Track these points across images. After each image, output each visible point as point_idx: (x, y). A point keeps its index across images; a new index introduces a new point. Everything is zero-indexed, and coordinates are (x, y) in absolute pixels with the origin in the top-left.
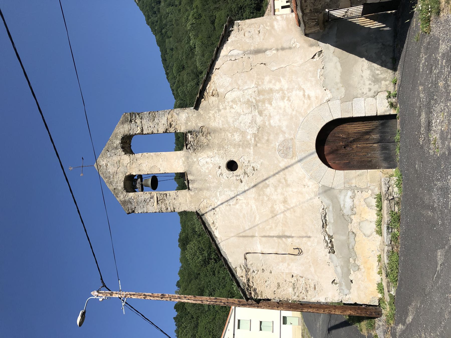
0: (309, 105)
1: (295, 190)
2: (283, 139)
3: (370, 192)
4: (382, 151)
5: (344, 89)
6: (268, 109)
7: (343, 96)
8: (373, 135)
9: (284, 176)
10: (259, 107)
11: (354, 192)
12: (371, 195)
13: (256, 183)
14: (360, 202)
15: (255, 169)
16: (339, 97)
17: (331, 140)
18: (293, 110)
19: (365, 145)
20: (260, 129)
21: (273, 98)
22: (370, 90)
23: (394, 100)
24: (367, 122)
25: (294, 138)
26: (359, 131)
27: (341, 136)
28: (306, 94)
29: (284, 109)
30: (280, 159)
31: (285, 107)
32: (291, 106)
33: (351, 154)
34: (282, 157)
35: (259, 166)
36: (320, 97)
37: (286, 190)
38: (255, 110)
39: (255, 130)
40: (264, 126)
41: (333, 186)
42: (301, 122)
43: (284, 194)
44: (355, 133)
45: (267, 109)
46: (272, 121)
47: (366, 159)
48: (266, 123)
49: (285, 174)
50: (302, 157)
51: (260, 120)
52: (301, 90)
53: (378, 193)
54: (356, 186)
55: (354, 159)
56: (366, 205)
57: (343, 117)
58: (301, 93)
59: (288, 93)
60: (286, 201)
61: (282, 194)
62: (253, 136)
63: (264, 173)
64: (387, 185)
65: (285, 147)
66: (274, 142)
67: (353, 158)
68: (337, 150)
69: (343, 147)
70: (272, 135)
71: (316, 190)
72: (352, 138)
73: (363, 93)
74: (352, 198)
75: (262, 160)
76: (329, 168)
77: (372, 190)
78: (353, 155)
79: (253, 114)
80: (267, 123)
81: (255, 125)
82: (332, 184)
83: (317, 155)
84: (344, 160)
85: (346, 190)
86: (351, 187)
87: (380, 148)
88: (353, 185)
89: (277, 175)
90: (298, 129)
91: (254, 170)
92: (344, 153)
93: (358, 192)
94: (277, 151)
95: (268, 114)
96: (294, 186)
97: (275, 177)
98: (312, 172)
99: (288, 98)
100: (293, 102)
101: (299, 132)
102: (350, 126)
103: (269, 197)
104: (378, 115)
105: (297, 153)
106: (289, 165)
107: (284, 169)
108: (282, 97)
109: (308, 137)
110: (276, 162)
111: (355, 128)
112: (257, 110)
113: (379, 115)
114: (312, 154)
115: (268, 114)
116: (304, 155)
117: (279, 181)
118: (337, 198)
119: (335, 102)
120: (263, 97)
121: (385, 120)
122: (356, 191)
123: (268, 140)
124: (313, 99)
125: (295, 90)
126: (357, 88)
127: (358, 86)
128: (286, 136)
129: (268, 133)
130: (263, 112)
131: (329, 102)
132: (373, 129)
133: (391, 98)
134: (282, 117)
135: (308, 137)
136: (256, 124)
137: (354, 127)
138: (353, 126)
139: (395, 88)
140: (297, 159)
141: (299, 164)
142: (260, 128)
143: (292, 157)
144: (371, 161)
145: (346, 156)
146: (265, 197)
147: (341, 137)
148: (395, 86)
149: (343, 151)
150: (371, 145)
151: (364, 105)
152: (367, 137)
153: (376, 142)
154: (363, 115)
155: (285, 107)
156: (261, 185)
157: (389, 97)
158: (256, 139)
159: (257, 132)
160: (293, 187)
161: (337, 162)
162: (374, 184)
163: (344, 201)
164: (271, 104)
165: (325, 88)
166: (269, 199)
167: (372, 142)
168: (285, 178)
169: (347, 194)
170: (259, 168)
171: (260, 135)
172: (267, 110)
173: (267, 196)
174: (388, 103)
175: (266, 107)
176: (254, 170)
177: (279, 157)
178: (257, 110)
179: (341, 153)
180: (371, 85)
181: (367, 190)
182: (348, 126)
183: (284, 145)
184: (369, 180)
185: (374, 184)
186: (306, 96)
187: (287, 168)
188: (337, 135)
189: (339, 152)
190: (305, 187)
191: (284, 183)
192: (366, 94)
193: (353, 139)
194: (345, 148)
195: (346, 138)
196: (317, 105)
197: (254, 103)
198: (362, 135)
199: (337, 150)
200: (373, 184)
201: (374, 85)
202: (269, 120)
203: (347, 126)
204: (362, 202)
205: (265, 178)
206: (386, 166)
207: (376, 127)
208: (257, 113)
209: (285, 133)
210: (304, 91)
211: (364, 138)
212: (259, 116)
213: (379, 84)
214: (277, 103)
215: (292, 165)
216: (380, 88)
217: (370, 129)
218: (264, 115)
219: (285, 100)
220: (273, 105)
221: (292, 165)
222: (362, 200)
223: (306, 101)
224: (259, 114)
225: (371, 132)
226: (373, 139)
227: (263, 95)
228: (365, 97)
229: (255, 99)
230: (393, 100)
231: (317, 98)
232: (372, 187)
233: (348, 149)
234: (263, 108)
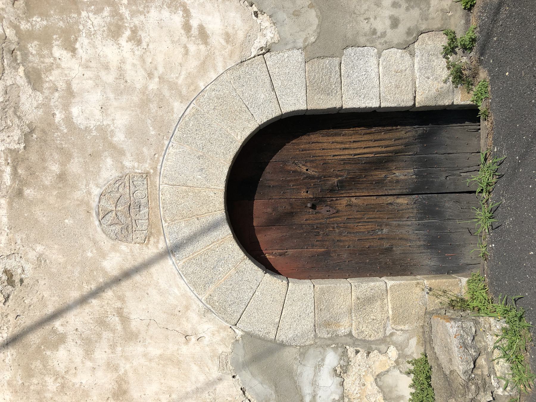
0: (204, 61)
1: (154, 351)
2: (115, 174)
3: (393, 352)
4: (421, 219)
5: (317, 16)
6: (63, 65)
7: (312, 39)
8: (397, 168)
9: (119, 304)
10: (31, 58)
11: (345, 353)
12: (397, 362)
13: (17, 330)
14: (364, 385)
15: (16, 279)
16: (301, 40)
17: (272, 183)
18: (150, 75)
19: (373, 200)
20: (35, 136)
21: (81, 27)
22: (395, 23)
23: (464, 59)
24: (380, 128)
25: (152, 171)
26: (355, 155)
27: (304, 169)
28: (194, 23)
29: (120, 69)
30: (106, 243)
31: (123, 61)
32: (142, 59)
33: (334, 228)
34: (114, 237)
35: (28, 267)
36: (241, 35)
37: (123, 351)
38: (14, 68)
39: (16, 138)
40: (50, 125)
41: (282, 337)
42: (176, 116)
43: (116, 368)
44: (346, 162)
45: (58, 66)
46: (75, 111)
47: (375, 244)
48: (54, 115)
49: (121, 299)
50: (180, 236)
51: (35, 104)
52: (176, 9)
53: (417, 356)
54: (350, 334)
55: (342, 244)
56: (381, 395)
57: (313, 106)
58: (178, 19)
59: (133, 14)
60: (125, 392)
61: (111, 366)
62: (6, 160)
63: (46, 294)
64: (472, 352)
65: (122, 200)
66: (84, 183)
67: (338, 238)
68: (291, 214)
69: (309, 205)
70: (76, 160)
71: (224, 349)
72: (337, 176)
73: (374, 32)
74: (338, 372)
75: (39, 248)
76: (268, 275)
77: (400, 347)
78: (337, 231)
79: (9, 83)
80: (59, 117)
81: (16, 121)
82: (275, 329)
83: (230, 232)
84: (313, 246)
85: (321, 349)
86: (337, 336)
87: (415, 211)
88: (343, 331)
89: (94, 302)
90: (166, 143)
91: (11, 282)
92: (312, 225)
93: (357, 352)
94: (94, 214)
95: (62, 85)
96: (151, 337)
97: (87, 309)
98: (212, 287)
99: (134, 31)
100: (151, 46)
101: (171, 150)
102: (331, 139)
103: (63, 378)
104: (417, 105)
105: (165, 225)
106: (136, 264)
107: (117, 281)
108: (112, 28)
109: (202, 170)
110: (89, 254)
111: (343, 146)
112: (21, 70)
113: (422, 104)
114: (213, 226)
115: (62, 85)
116: (186, 231)
117: (102, 322)
118: (291, 374)
119: (286, 55)
120: (45, 23)
121: (430, 125)
122: (351, 351)
123: (62, 177)
124: (216, 40)
125: (156, 7)
126: (355, 13)
127: (358, 7)
128: (127, 164)
129: (61, 150)
130: (43, 76)
131: (267, 56)
132: (396, 152)
133: (456, 54)
134: (111, 96)
135: (202, 170)
136: (19, 117)
137: (342, 143)
138: (339, 139)
139: (468, 22)
140: (162, 246)
141: (170, 262)
142: (32, 131)
143: (147, 238)
144: (389, 250)
145: (318, 234)
146: (49, 380)
147: (304, 173)
148: (468, 15)
149: (307, 216)
150: (390, 199)
151: (376, 70)
152: (380, 174)
153: (404, 191)
154: (374, 104)
155: (123, 61)
156: (34, 338)
157: (450, 50)
158: (20, 171)
159: (23, 145)
160: (148, 341)
161: (290, 252)
162: (406, 327)
163: (314, 383)
164: (74, 50)
165: (255, 8)
166: (63, 386)
167: (394, 192)
168: (120, 312)
169: (323, 360)
170: (29, 275)
171: (33, 157)
172: (60, 71)
173: (57, 375)
174: (449, 68)
175: (55, 59)
176: (11, 282)
177: (100, 236)
178: (21, 70)
179: (302, 225)
180: (400, 6)
181: (383, 347)
182: (325, 139)
183: (118, 195)
184: (390, 312)
185: (406, 327)
186: (195, 31)
187: (127, 275)
188: (291, 167)
189: (297, 220)
190: (187, 341)
191: (119, 327)
192: (384, 34)
193: (339, 181)
194: (314, 207)
195: (318, 178)
196: (231, 64)
197: (10, 42)
198: (365, 170)
199: (291, 214)
200: (402, 327)
201: (407, 9)
202: (66, 107)
203: (321, 139)
204: (371, 387)
205: (50, 310)
206: (432, 264)
207: (406, 145)
208: (24, 78)
209: (122, 153)
210: (187, 13)
211: (370, 178)
212: (30, 91)
213: (422, 6)
214: (95, 47)
215: (146, 265)
216: (427, 19)
217: (387, 152)
218: (47, 84)
219: (123, 40)
220: (80, 52)
221: (146, 265)
222: (370, 379)
223: (192, 48)
224: (29, 82)
225: (392, 161)
226: (398, 181)
227: (44, 15)
228: (379, 46)
229: (16, 28)
230: (463, 61)
231: (228, 38)
232: (399, 337)
233: (323, 210)
234: (43, 63)
